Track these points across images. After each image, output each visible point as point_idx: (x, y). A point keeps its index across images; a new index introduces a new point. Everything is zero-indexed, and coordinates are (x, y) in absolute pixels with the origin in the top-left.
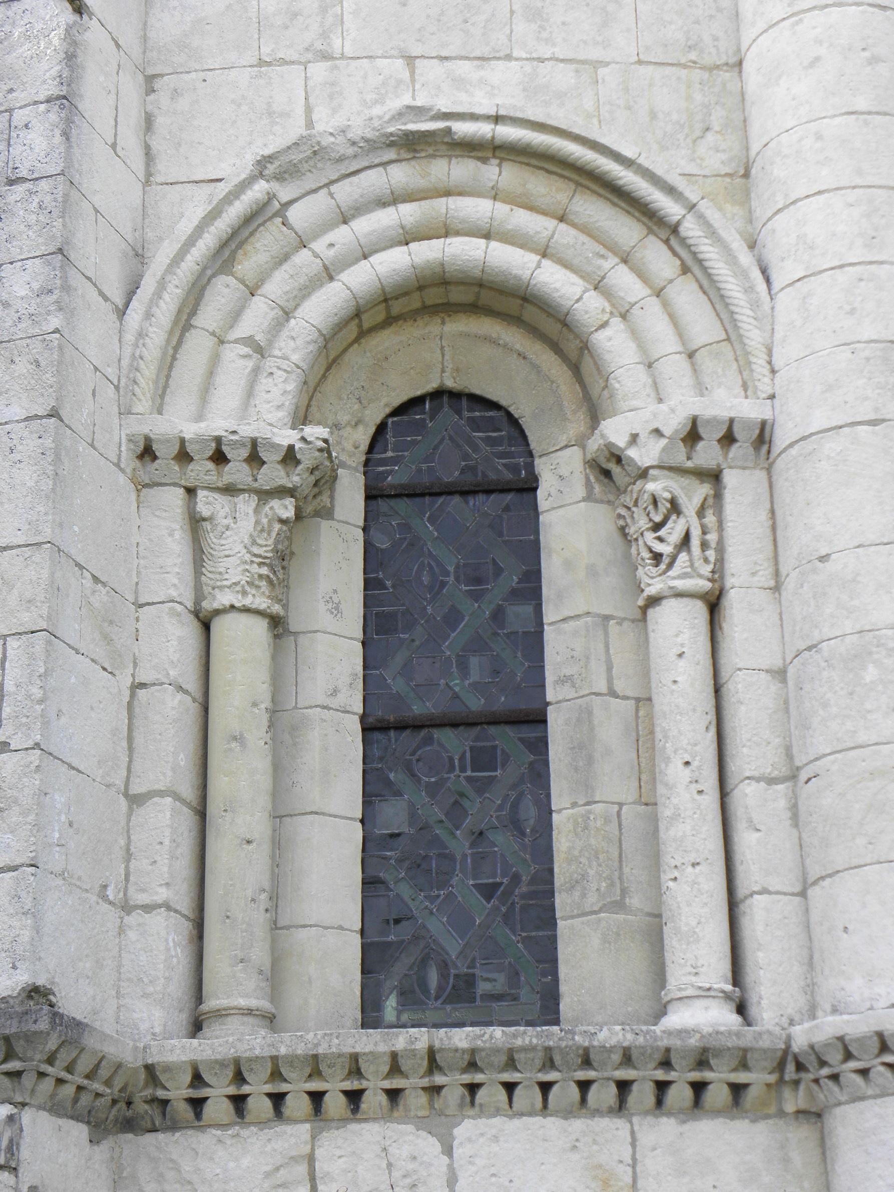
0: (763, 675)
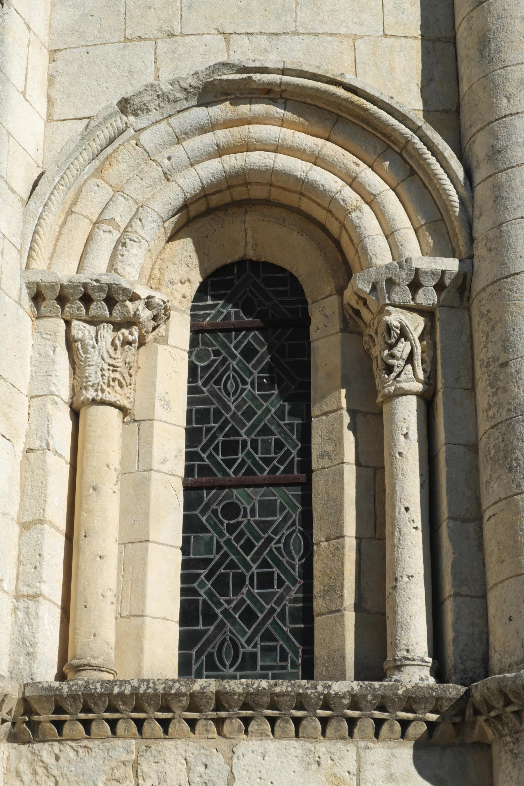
0: (462, 448)
